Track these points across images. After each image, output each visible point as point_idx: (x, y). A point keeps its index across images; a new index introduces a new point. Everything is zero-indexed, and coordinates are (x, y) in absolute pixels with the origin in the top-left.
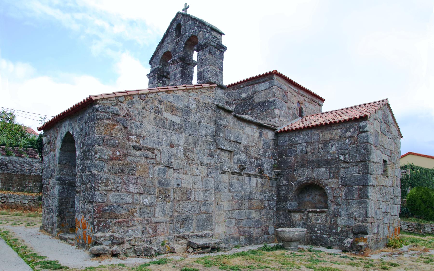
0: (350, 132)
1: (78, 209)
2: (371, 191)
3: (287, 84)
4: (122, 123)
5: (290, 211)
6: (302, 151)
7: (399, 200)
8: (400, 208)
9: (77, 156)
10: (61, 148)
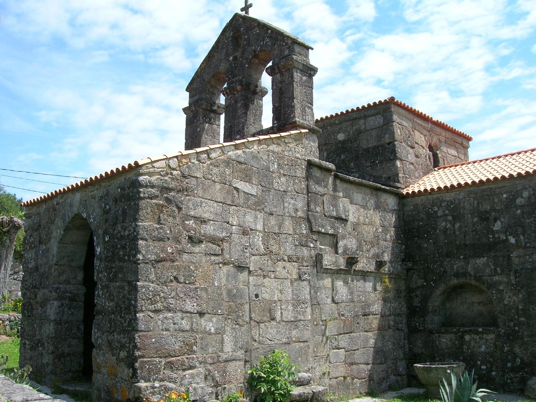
0: (522, 197)
6: (445, 231)
9: (98, 254)
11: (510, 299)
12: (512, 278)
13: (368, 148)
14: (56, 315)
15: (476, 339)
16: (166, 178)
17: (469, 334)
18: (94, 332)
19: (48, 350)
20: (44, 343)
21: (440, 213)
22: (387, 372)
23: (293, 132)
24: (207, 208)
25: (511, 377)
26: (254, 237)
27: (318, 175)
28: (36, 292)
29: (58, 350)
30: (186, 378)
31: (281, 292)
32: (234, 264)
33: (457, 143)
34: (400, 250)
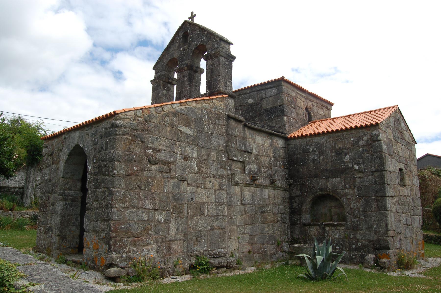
0: (363, 140)
1: (88, 227)
2: (389, 202)
3: (294, 89)
4: (139, 138)
5: (305, 225)
6: (314, 161)
7: (419, 211)
8: (421, 219)
9: (89, 171)
10: (66, 161)
11: (354, 204)
12: (356, 191)
13: (267, 109)
14: (61, 210)
15: (333, 229)
16: (134, 122)
17: (328, 227)
18: (85, 221)
19: (55, 233)
20: (53, 229)
21: (311, 150)
22: (276, 249)
23: (218, 96)
24: (161, 142)
25: (355, 254)
26: (191, 162)
27: (234, 124)
28: (49, 196)
29: (62, 234)
30: (144, 251)
31: (208, 197)
32: (178, 178)
33: (324, 107)
34: (286, 173)
